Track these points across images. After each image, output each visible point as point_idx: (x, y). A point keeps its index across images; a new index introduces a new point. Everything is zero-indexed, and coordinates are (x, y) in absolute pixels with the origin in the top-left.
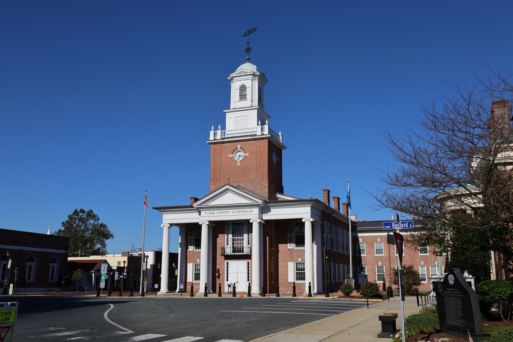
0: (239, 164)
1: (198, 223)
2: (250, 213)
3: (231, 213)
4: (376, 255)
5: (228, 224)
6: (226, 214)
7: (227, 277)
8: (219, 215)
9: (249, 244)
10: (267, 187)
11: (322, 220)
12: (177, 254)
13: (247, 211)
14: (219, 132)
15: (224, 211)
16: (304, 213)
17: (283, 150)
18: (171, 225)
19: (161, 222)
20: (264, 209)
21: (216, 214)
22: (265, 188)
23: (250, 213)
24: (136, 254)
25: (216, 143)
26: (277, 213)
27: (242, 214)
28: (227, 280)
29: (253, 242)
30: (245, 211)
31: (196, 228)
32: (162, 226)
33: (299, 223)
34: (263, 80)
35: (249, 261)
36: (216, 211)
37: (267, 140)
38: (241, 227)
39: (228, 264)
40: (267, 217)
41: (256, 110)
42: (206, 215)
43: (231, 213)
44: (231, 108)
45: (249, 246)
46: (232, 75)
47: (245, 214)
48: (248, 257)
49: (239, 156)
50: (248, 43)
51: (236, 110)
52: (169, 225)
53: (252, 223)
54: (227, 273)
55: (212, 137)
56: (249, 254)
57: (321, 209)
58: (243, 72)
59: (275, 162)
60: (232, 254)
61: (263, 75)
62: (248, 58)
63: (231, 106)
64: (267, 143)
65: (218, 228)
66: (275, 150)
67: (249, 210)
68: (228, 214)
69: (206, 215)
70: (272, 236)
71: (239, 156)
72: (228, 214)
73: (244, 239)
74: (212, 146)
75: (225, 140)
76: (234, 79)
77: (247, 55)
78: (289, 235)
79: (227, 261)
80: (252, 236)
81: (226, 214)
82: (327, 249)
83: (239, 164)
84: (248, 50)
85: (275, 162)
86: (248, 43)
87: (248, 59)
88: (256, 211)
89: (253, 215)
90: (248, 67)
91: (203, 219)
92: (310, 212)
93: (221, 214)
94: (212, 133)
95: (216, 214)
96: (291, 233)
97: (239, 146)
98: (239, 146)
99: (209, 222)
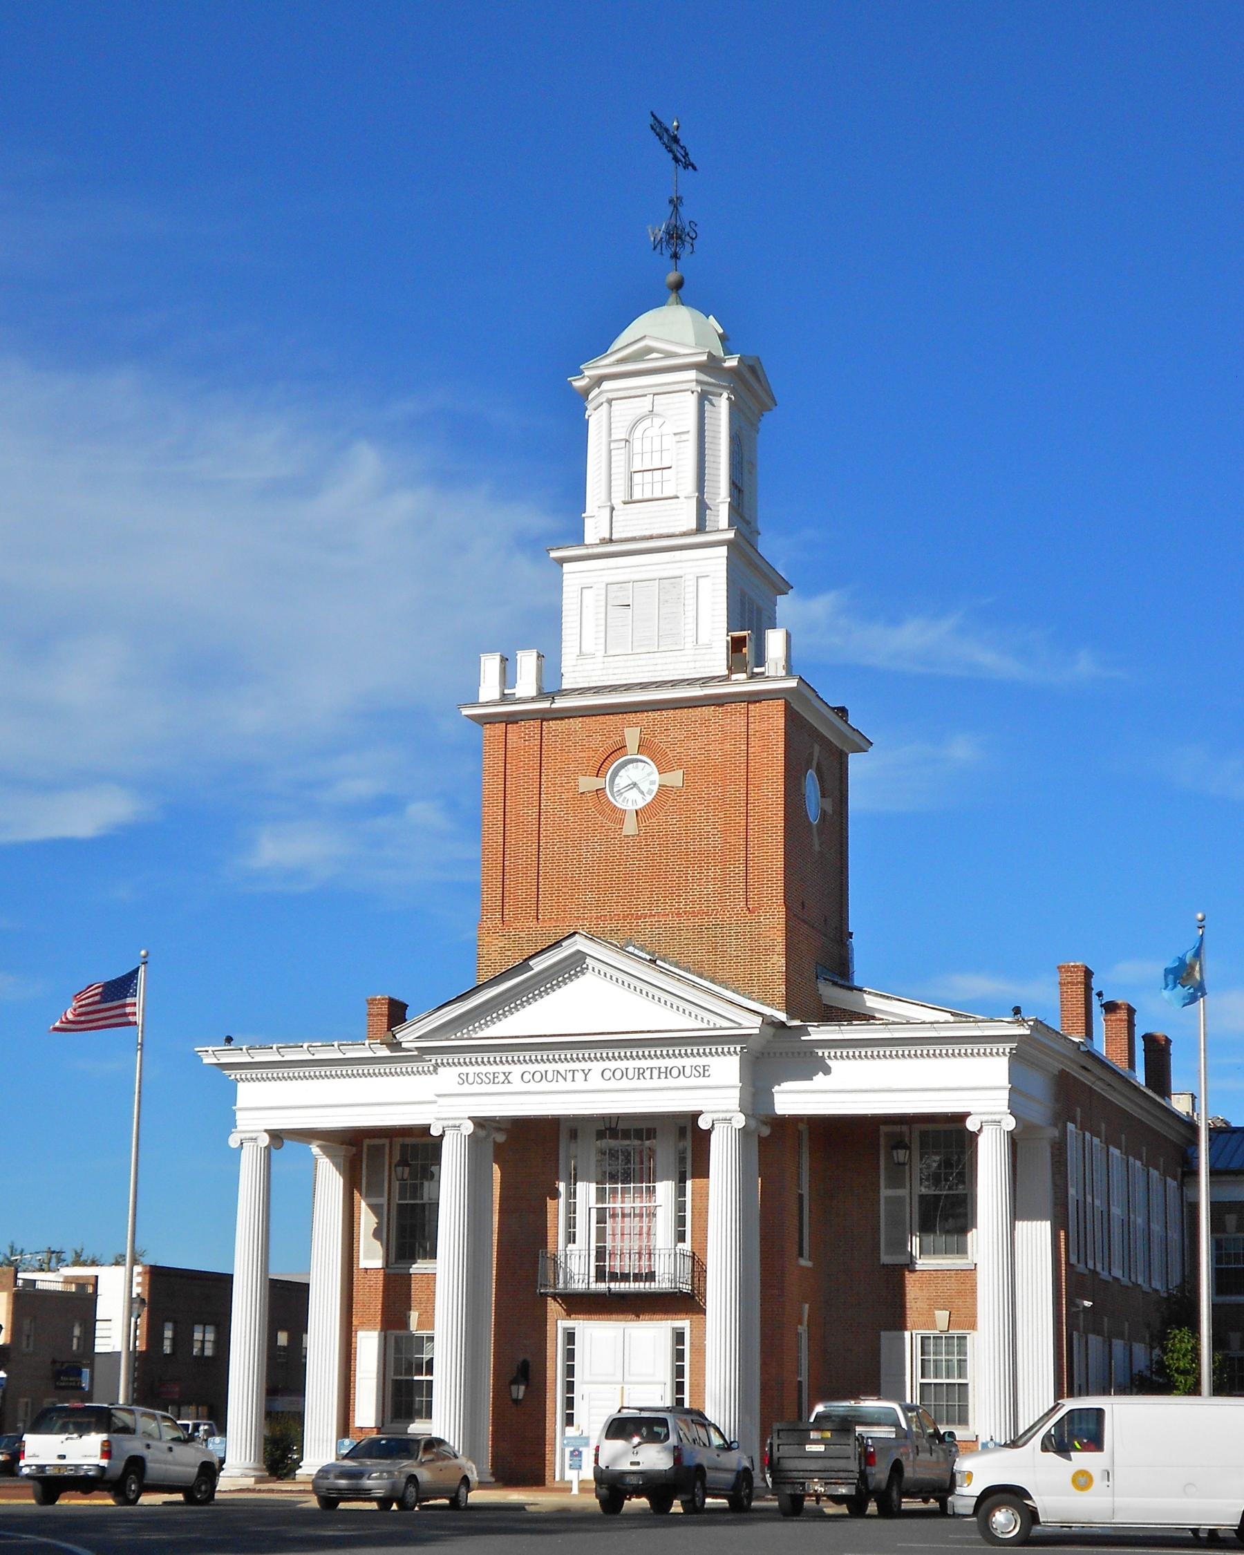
0: (630, 827)
1: (427, 1128)
2: (693, 1082)
3: (595, 1081)
4: (190, 1422)
5: (574, 1135)
6: (569, 1085)
7: (570, 1403)
8: (533, 1086)
9: (681, 1237)
10: (780, 948)
11: (1062, 1116)
12: (226, 1281)
13: (682, 1071)
14: (527, 663)
15: (561, 1067)
16: (976, 1088)
17: (855, 762)
18: (277, 1137)
19: (230, 1123)
20: (772, 1057)
21: (517, 1085)
22: (769, 950)
23: (693, 1082)
24: (50, 1281)
25: (510, 719)
26: (850, 1085)
27: (656, 1083)
28: (569, 1420)
29: (707, 1227)
30: (668, 1072)
31: (412, 1151)
32: (233, 1142)
33: (948, 1138)
34: (745, 389)
35: (684, 1323)
36: (516, 1070)
37: (586, 542)
38: (652, 1147)
39: (570, 1337)
40: (793, 1099)
41: (723, 551)
42: (466, 1088)
43: (595, 1081)
44: (591, 536)
45: (687, 1246)
46: (591, 370)
47: (670, 1082)
48: (685, 1302)
49: (636, 784)
50: (676, 203)
51: (613, 548)
52: (265, 1140)
53: (708, 1132)
54: (570, 1387)
55: (489, 689)
56: (687, 1288)
57: (1056, 1066)
58: (650, 350)
59: (814, 818)
60: (593, 1286)
61: (752, 369)
62: (672, 277)
63: (589, 525)
64: (781, 723)
65: (528, 1154)
66: (817, 749)
67: (688, 1062)
68: (580, 1083)
69: (466, 1088)
70: (801, 1196)
71: (636, 784)
72: (580, 1083)
73: (659, 1211)
74: (488, 730)
75: (560, 703)
76: (606, 385)
77: (675, 264)
78: (885, 1192)
79: (569, 1323)
80: (702, 1198)
81: (569, 1085)
82: (1081, 1267)
83: (630, 827)
84: (676, 236)
85: (814, 818)
86: (676, 203)
87: (678, 286)
88: (727, 1069)
89: (713, 1092)
90: (675, 331)
91: (441, 1099)
92: (1005, 1082)
93: (544, 1086)
94: (490, 666)
95: (517, 1085)
96: (896, 1180)
97: (632, 737)
98: (632, 737)
99: (481, 1123)
